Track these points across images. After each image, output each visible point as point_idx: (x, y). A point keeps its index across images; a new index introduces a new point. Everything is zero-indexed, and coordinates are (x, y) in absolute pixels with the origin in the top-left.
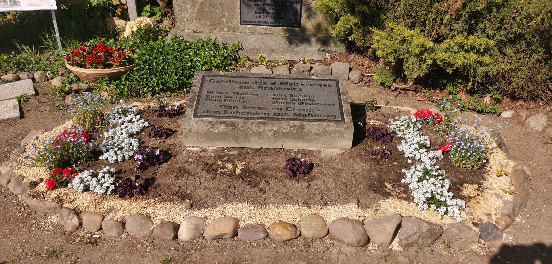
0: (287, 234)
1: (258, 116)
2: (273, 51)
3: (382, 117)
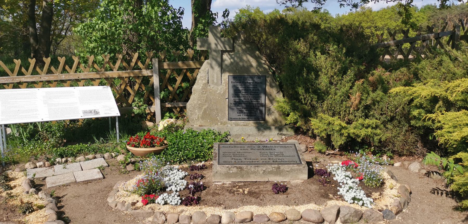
0: (280, 218)
1: (254, 163)
2: (249, 135)
3: (323, 166)
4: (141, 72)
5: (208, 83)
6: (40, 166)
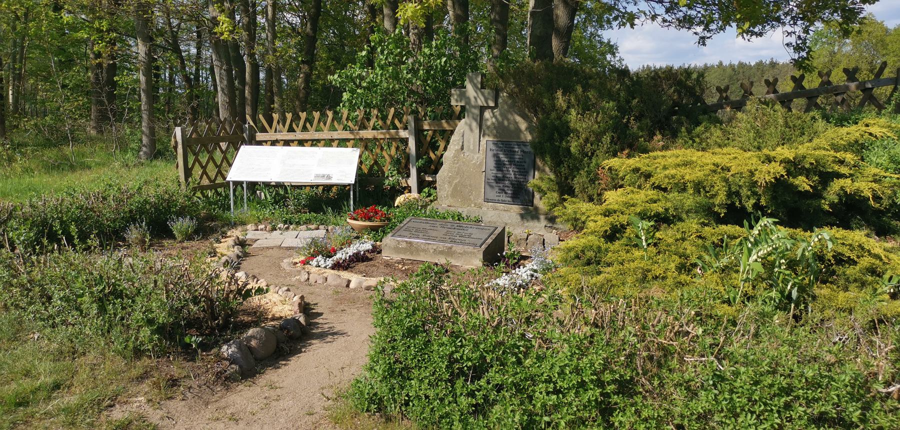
4: (397, 133)
5: (462, 148)
6: (262, 230)
